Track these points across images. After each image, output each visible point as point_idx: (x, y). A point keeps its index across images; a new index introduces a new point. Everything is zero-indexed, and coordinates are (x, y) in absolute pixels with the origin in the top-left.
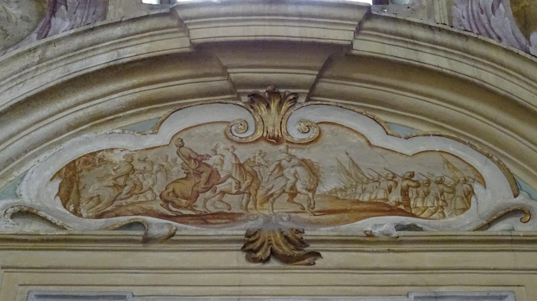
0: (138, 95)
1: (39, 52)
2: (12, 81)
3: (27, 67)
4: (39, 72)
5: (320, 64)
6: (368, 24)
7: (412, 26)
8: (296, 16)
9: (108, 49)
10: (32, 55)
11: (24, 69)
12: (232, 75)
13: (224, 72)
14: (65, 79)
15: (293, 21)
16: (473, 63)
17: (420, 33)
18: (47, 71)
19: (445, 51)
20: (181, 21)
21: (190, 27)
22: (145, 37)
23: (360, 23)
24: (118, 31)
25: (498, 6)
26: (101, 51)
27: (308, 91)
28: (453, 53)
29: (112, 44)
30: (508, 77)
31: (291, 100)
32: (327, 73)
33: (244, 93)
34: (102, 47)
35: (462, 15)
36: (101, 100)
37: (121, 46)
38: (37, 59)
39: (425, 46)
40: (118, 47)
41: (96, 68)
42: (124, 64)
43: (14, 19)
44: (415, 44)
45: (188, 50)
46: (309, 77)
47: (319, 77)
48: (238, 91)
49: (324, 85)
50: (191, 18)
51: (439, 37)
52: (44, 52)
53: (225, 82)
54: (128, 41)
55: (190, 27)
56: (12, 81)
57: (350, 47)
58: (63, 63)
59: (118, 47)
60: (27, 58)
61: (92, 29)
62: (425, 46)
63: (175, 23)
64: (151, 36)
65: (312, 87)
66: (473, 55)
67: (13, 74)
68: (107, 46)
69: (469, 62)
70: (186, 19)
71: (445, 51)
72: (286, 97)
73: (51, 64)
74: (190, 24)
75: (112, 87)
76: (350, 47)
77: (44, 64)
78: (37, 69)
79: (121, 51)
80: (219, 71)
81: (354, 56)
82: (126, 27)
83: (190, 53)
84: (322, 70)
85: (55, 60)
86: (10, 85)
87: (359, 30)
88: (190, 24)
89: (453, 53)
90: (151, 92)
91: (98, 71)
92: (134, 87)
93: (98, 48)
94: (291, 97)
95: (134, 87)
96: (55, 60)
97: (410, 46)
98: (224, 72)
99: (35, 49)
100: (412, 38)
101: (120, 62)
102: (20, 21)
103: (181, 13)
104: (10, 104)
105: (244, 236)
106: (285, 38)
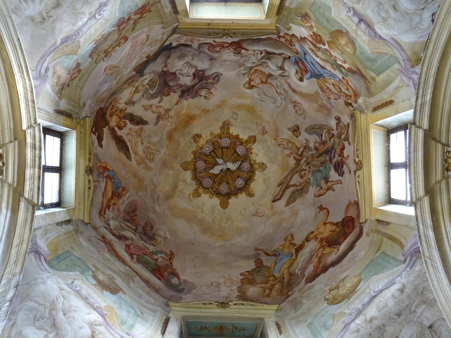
0: (447, 219)
1: (427, 259)
2: (437, 272)
3: (432, 265)
4: (435, 260)
5: (434, 143)
6: (418, 124)
7: (417, 105)
8: (415, 153)
9: (428, 230)
10: (428, 263)
11: (433, 266)
12: (439, 179)
13: (439, 182)
14: (437, 249)
15: (417, 154)
16: (429, 79)
17: (419, 102)
18: (434, 257)
19: (426, 91)
20: (417, 200)
21: (420, 197)
22: (424, 215)
23: (417, 127)
24: (421, 226)
25: (416, 72)
26: (428, 233)
27: (446, 147)
28: (426, 88)
29: (426, 229)
30: (433, 62)
31: (449, 154)
32: (438, 139)
33: (447, 174)
34: (427, 233)
35: (194, 81)
36: (449, 235)
37: (427, 225)
38: (429, 261)
39: (424, 100)
40: (427, 227)
41: (434, 236)
42: (433, 225)
43: (420, 269)
44: (424, 104)
45: (428, 197)
46: (439, 146)
47: (440, 142)
48: (446, 176)
49: (444, 140)
50: (416, 196)
51: (420, 94)
52: (427, 257)
53: (443, 182)
54: (425, 222)
55: (420, 197)
56: (437, 272)
57: (425, 130)
58: (432, 250)
59: (427, 227)
60: (429, 265)
61: (420, 237)
62: (424, 100)
63: (419, 203)
64: (423, 213)
65: (444, 145)
66: (426, 79)
67: (434, 271)
68: (427, 231)
69: (429, 80)
70: (416, 198)
71: (426, 91)
72: (448, 156)
73: (432, 255)
74: (418, 196)
75: (443, 230)
76: (425, 130)
77: (431, 258)
78: (433, 261)
79: (428, 225)
80: (438, 185)
81: (429, 128)
82: (420, 222)
83: (430, 196)
84: (436, 141)
85: (430, 253)
86: (439, 273)
87: (420, 127)
88: (418, 196)
89: (426, 88)
90: (446, 214)
91: (435, 236)
92: (444, 220)
93: (427, 234)
94: (448, 154)
95: (444, 220)
96: (430, 253)
97: (425, 105)
98: (439, 182)
99: (426, 261)
100: (421, 105)
101: (432, 226)
102: (422, 266)
103: (414, 200)
104: (445, 274)
105: (44, 164)
106: (423, 157)
